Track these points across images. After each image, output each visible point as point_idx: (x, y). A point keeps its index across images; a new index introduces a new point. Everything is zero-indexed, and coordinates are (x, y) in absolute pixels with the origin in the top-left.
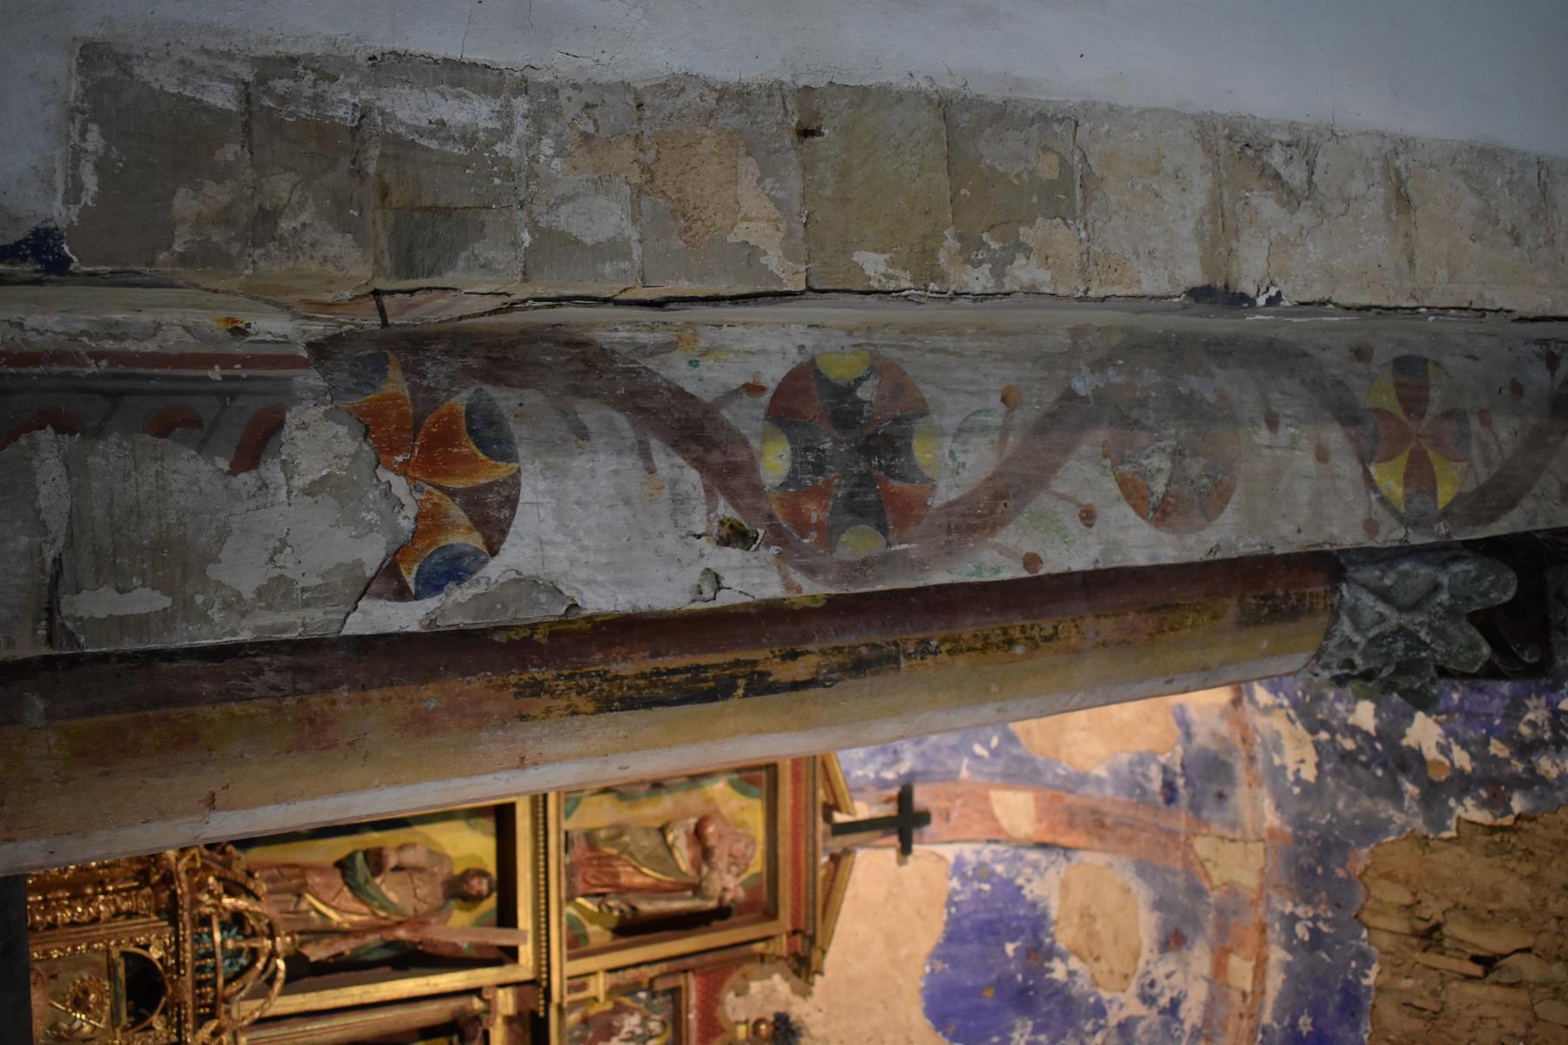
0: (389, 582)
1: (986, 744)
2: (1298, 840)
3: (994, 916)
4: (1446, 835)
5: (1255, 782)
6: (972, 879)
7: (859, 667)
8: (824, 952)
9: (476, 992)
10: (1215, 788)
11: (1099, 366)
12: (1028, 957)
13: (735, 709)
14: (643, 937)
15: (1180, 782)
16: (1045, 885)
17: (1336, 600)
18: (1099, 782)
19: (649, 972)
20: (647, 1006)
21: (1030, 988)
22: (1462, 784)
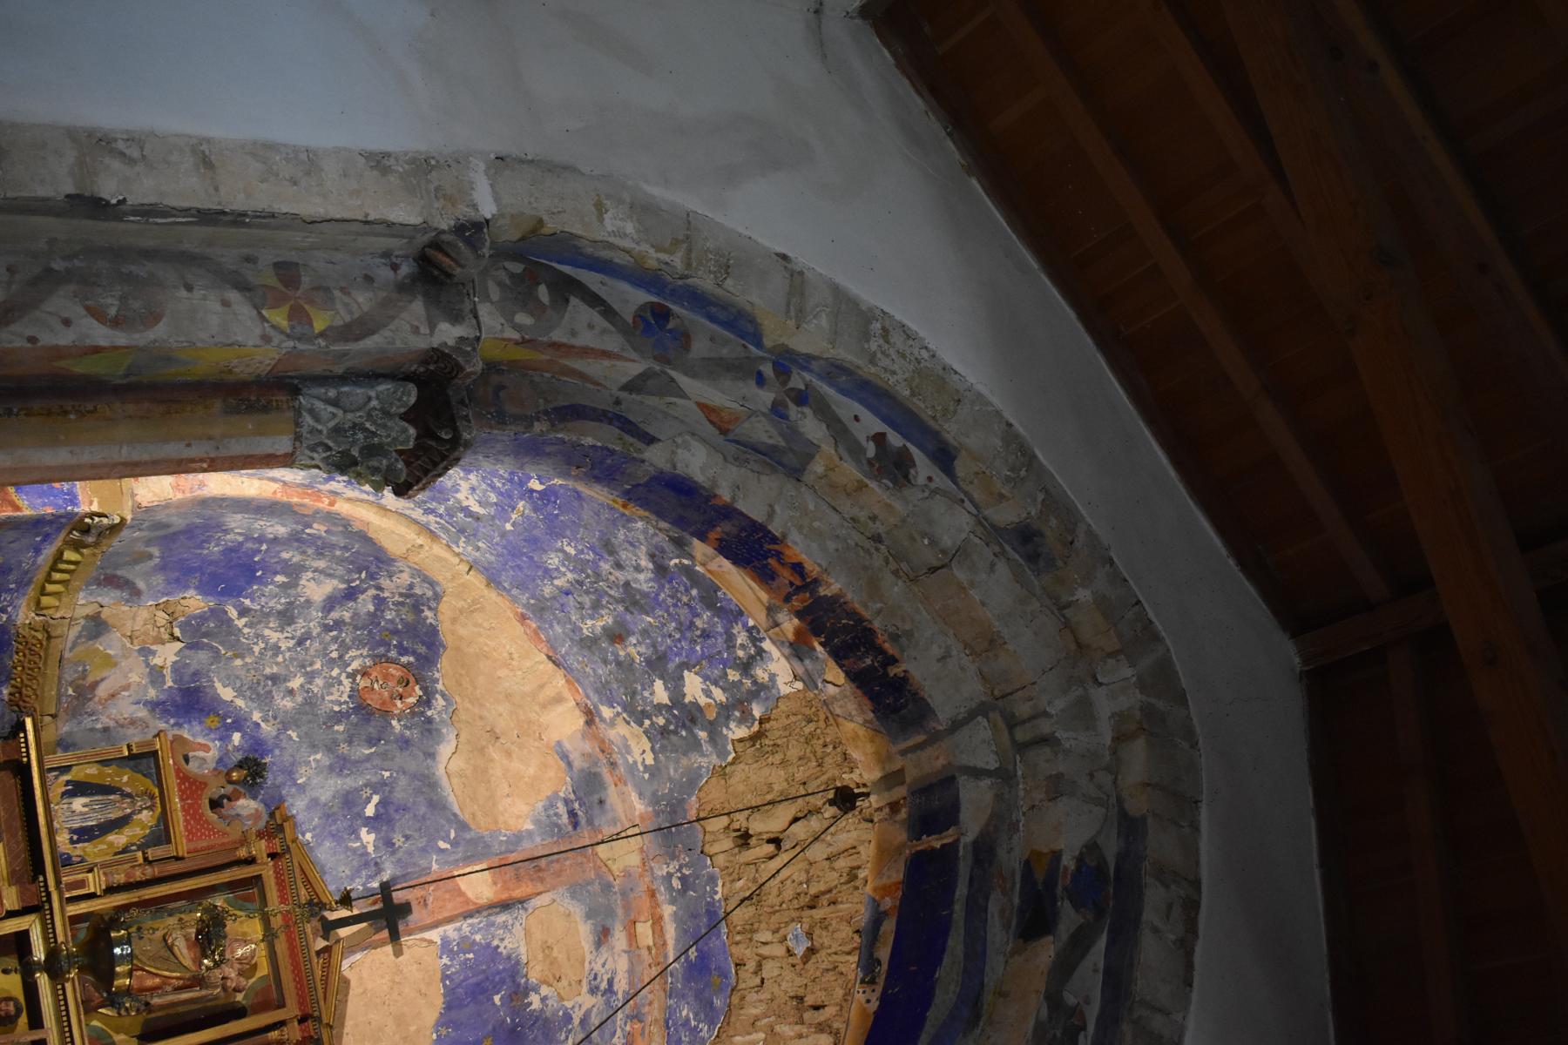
1: (446, 839)
2: (657, 814)
3: (481, 977)
4: (730, 758)
5: (620, 781)
10: (596, 797)
11: (64, 258)
15: (576, 805)
16: (514, 938)
17: (297, 404)
18: (530, 833)
22: (725, 711)
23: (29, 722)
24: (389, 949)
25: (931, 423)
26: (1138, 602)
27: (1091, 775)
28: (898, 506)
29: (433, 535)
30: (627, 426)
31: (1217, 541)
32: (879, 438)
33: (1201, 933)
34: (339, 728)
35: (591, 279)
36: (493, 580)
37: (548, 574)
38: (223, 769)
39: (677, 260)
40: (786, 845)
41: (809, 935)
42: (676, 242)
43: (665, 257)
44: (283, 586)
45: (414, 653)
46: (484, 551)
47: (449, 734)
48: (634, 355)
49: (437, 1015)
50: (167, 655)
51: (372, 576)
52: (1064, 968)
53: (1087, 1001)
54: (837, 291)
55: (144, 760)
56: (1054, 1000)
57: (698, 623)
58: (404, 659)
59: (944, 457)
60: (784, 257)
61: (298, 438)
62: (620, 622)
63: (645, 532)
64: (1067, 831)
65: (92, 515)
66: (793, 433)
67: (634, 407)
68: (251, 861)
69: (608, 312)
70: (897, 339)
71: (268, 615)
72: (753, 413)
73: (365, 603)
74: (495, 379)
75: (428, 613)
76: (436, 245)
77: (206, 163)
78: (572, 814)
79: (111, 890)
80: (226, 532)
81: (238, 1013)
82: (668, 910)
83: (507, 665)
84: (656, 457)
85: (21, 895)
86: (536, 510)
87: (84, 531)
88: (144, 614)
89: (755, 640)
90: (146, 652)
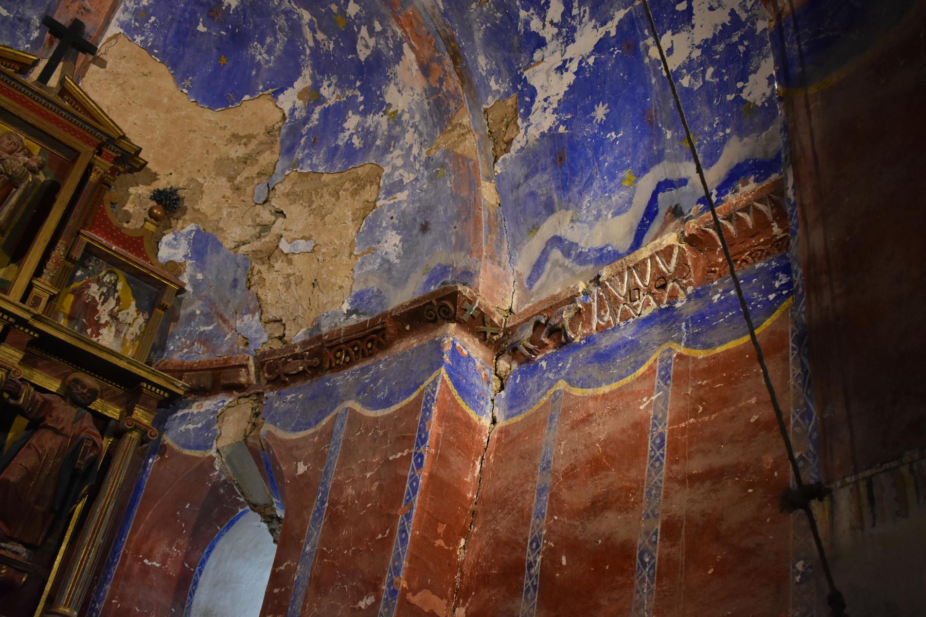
3: (174, 25)
6: (142, 26)
8: (124, 137)
12: (213, 18)
14: (17, 218)
19: (59, 251)
20: (89, 275)
21: (234, 29)
24: (93, 67)
49: (171, 78)
81: (53, 189)
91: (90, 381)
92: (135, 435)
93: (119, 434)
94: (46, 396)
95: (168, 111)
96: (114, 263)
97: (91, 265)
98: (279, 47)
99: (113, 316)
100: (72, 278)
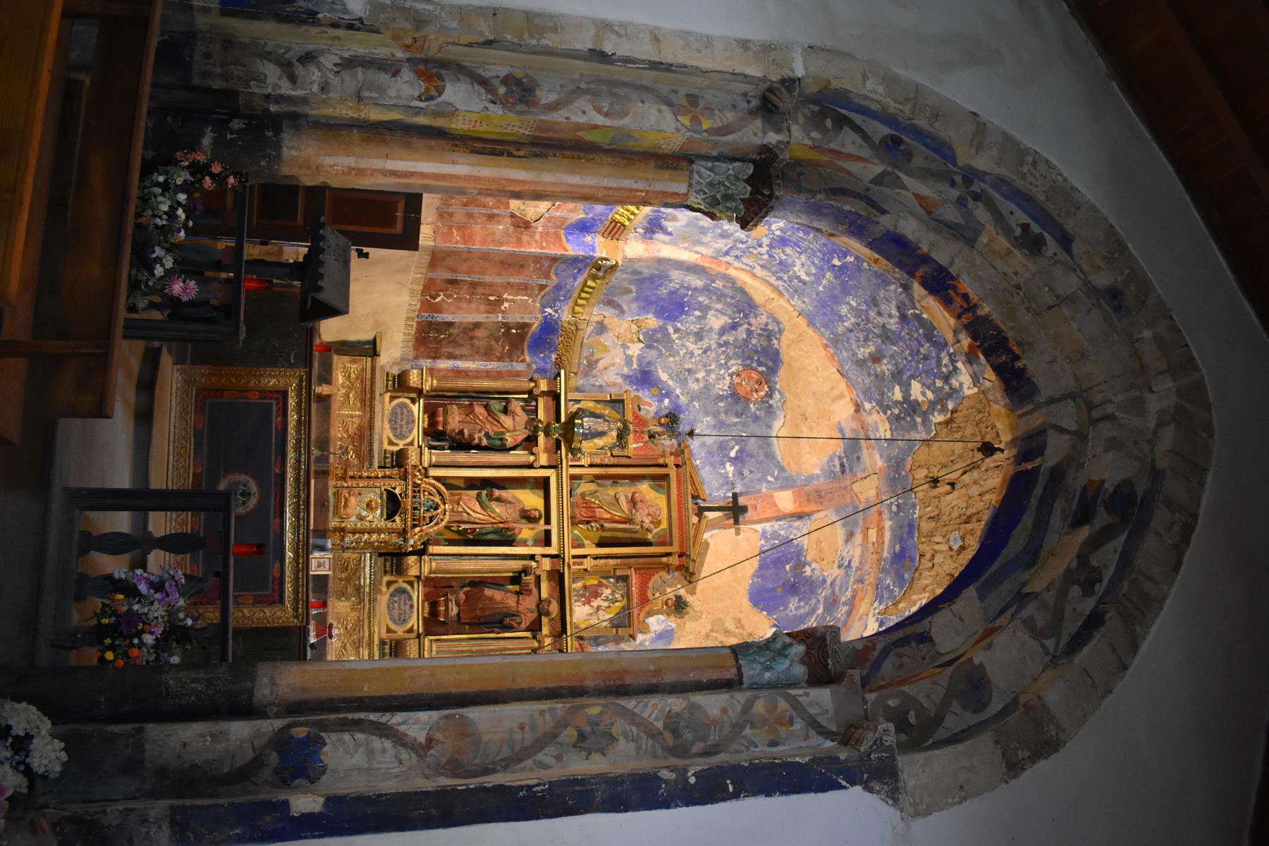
0: (420, 98)
1: (772, 475)
2: (888, 467)
7: (536, 156)
9: (532, 557)
11: (588, 83)
13: (504, 160)
18: (818, 476)
19: (611, 562)
22: (932, 404)
23: (562, 372)
24: (733, 531)
25: (1058, 219)
26: (1187, 345)
27: (1136, 443)
28: (1031, 266)
29: (780, 294)
30: (871, 203)
31: (1256, 321)
32: (1025, 227)
33: (1191, 545)
34: (721, 404)
35: (858, 118)
36: (811, 323)
37: (841, 319)
38: (657, 417)
39: (907, 109)
40: (957, 486)
41: (963, 538)
42: (907, 100)
43: (900, 107)
44: (698, 318)
45: (766, 365)
46: (807, 304)
47: (780, 414)
48: (876, 161)
50: (635, 349)
51: (746, 316)
52: (1093, 544)
53: (1106, 566)
54: (1006, 137)
55: (617, 403)
56: (1082, 559)
57: (922, 350)
58: (760, 369)
59: (1066, 242)
60: (975, 114)
61: (690, 185)
62: (879, 350)
63: (895, 291)
64: (1106, 469)
65: (602, 259)
66: (969, 215)
67: (876, 192)
68: (665, 466)
69: (865, 137)
70: (1042, 168)
71: (689, 334)
72: (945, 202)
73: (741, 333)
74: (799, 169)
75: (775, 342)
76: (770, 90)
77: (656, 39)
78: (842, 465)
79: (591, 466)
80: (671, 281)
82: (888, 524)
83: (814, 375)
84: (886, 222)
85: (549, 458)
86: (836, 278)
87: (600, 269)
88: (625, 325)
89: (953, 361)
90: (624, 346)
91: (554, 608)
92: (536, 645)
93: (534, 637)
94: (535, 591)
95: (734, 580)
96: (628, 595)
97: (620, 584)
98: (802, 611)
99: (598, 608)
100: (607, 578)
